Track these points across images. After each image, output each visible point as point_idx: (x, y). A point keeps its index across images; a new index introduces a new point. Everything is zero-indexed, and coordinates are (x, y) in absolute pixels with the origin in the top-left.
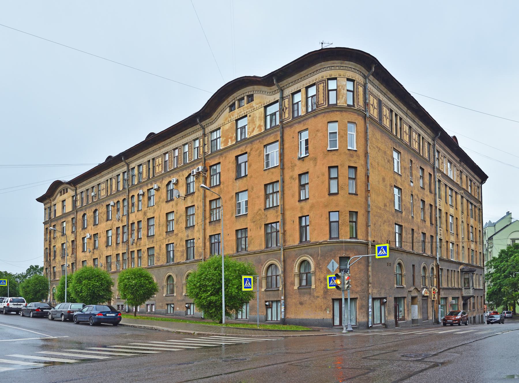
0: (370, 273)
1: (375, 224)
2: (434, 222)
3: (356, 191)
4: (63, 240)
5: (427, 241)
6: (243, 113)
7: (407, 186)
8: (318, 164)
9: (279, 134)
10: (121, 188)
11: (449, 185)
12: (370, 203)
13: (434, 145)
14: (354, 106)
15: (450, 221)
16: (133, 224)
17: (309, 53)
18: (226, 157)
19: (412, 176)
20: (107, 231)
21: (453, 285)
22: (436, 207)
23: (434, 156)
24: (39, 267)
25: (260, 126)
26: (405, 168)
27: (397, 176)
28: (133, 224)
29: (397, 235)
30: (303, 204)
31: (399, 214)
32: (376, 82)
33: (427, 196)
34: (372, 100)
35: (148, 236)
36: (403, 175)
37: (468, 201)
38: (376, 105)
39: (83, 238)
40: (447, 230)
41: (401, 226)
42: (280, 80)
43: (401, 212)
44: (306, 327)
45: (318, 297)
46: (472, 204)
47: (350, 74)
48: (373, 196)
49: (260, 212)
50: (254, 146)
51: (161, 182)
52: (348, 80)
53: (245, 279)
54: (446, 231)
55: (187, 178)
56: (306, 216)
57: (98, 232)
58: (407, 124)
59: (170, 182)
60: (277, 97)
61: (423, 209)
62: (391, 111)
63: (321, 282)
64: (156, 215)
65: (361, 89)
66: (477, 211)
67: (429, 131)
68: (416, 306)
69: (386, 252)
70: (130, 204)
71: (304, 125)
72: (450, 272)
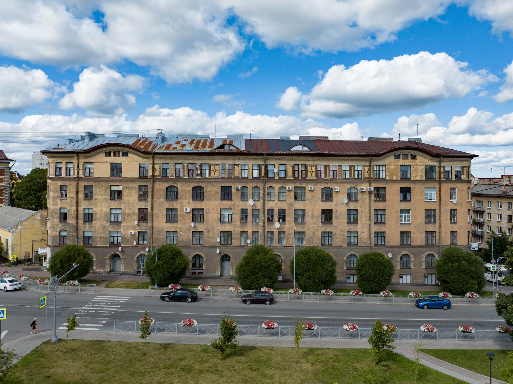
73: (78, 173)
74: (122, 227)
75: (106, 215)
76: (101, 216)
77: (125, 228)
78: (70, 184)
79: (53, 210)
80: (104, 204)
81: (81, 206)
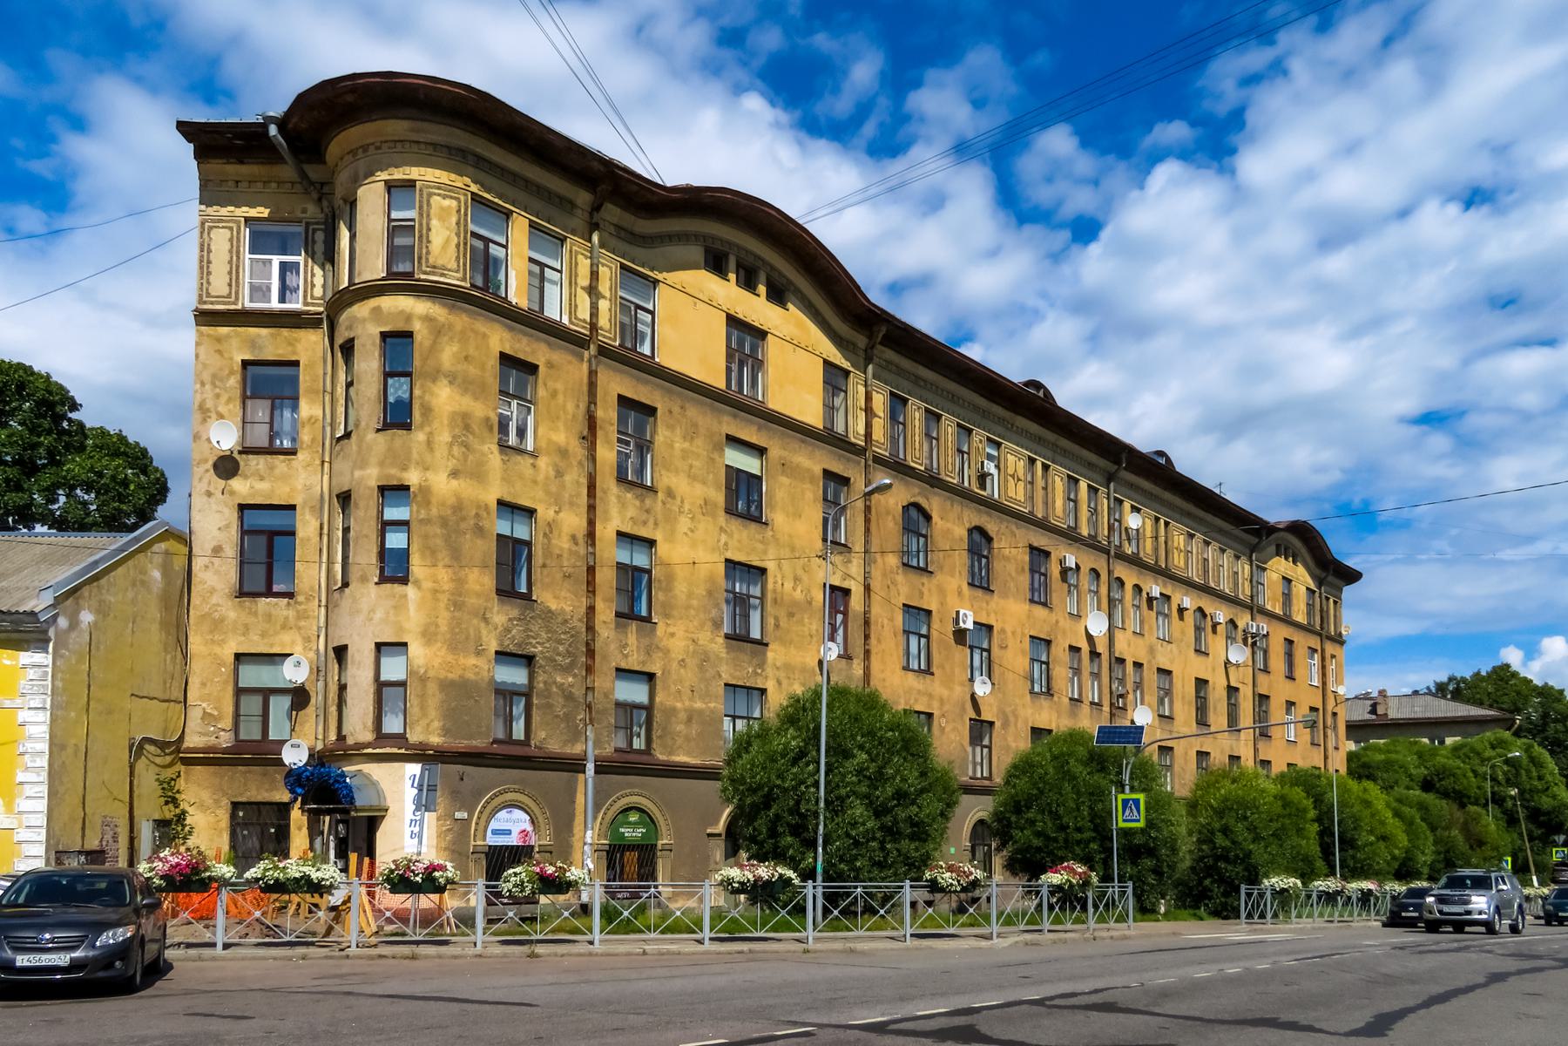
21: (519, 731)
42: (888, 341)
44: (640, 597)
53: (1125, 802)
60: (1300, 617)
68: (1474, 899)
73: (868, 426)
74: (769, 671)
75: (710, 593)
76: (690, 595)
77: (782, 675)
78: (550, 365)
79: (458, 507)
80: (701, 527)
81: (607, 519)
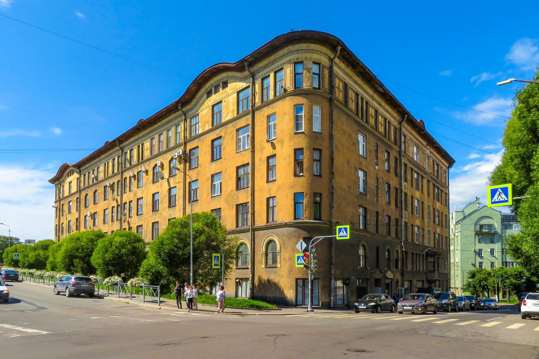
0: (333, 254)
1: (339, 206)
2: (399, 205)
3: (320, 172)
4: (70, 217)
5: (392, 224)
6: (218, 98)
7: (372, 169)
8: (285, 146)
9: (250, 116)
10: (116, 171)
11: (415, 169)
12: (334, 185)
13: (401, 129)
14: (319, 88)
15: (416, 205)
16: (126, 203)
17: (277, 38)
18: (203, 141)
19: (377, 159)
20: (105, 210)
22: (401, 190)
23: (400, 139)
24: (115, 231)
25: (233, 111)
26: (370, 151)
27: (362, 159)
28: (125, 203)
29: (361, 217)
30: (271, 184)
31: (364, 197)
32: (342, 65)
33: (392, 179)
34: (338, 83)
35: (137, 215)
36: (368, 158)
37: (434, 185)
38: (341, 87)
39: (86, 216)
40: (412, 213)
41: (365, 209)
42: (251, 65)
43: (366, 195)
45: (283, 276)
46: (438, 188)
47: (316, 57)
48: (337, 178)
49: (232, 193)
50: (228, 130)
51: (149, 165)
52: (314, 63)
53: (215, 257)
54: (411, 214)
55: (170, 162)
56: (273, 197)
57: (97, 211)
58: (373, 108)
59: (156, 165)
61: (389, 191)
62: (357, 95)
63: (286, 261)
64: (144, 196)
65: (326, 72)
66: (444, 196)
67: (395, 115)
69: (347, 233)
70: (123, 185)
71: (272, 109)
72: (415, 255)
